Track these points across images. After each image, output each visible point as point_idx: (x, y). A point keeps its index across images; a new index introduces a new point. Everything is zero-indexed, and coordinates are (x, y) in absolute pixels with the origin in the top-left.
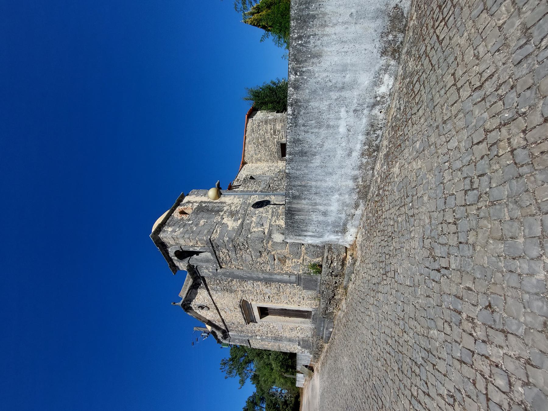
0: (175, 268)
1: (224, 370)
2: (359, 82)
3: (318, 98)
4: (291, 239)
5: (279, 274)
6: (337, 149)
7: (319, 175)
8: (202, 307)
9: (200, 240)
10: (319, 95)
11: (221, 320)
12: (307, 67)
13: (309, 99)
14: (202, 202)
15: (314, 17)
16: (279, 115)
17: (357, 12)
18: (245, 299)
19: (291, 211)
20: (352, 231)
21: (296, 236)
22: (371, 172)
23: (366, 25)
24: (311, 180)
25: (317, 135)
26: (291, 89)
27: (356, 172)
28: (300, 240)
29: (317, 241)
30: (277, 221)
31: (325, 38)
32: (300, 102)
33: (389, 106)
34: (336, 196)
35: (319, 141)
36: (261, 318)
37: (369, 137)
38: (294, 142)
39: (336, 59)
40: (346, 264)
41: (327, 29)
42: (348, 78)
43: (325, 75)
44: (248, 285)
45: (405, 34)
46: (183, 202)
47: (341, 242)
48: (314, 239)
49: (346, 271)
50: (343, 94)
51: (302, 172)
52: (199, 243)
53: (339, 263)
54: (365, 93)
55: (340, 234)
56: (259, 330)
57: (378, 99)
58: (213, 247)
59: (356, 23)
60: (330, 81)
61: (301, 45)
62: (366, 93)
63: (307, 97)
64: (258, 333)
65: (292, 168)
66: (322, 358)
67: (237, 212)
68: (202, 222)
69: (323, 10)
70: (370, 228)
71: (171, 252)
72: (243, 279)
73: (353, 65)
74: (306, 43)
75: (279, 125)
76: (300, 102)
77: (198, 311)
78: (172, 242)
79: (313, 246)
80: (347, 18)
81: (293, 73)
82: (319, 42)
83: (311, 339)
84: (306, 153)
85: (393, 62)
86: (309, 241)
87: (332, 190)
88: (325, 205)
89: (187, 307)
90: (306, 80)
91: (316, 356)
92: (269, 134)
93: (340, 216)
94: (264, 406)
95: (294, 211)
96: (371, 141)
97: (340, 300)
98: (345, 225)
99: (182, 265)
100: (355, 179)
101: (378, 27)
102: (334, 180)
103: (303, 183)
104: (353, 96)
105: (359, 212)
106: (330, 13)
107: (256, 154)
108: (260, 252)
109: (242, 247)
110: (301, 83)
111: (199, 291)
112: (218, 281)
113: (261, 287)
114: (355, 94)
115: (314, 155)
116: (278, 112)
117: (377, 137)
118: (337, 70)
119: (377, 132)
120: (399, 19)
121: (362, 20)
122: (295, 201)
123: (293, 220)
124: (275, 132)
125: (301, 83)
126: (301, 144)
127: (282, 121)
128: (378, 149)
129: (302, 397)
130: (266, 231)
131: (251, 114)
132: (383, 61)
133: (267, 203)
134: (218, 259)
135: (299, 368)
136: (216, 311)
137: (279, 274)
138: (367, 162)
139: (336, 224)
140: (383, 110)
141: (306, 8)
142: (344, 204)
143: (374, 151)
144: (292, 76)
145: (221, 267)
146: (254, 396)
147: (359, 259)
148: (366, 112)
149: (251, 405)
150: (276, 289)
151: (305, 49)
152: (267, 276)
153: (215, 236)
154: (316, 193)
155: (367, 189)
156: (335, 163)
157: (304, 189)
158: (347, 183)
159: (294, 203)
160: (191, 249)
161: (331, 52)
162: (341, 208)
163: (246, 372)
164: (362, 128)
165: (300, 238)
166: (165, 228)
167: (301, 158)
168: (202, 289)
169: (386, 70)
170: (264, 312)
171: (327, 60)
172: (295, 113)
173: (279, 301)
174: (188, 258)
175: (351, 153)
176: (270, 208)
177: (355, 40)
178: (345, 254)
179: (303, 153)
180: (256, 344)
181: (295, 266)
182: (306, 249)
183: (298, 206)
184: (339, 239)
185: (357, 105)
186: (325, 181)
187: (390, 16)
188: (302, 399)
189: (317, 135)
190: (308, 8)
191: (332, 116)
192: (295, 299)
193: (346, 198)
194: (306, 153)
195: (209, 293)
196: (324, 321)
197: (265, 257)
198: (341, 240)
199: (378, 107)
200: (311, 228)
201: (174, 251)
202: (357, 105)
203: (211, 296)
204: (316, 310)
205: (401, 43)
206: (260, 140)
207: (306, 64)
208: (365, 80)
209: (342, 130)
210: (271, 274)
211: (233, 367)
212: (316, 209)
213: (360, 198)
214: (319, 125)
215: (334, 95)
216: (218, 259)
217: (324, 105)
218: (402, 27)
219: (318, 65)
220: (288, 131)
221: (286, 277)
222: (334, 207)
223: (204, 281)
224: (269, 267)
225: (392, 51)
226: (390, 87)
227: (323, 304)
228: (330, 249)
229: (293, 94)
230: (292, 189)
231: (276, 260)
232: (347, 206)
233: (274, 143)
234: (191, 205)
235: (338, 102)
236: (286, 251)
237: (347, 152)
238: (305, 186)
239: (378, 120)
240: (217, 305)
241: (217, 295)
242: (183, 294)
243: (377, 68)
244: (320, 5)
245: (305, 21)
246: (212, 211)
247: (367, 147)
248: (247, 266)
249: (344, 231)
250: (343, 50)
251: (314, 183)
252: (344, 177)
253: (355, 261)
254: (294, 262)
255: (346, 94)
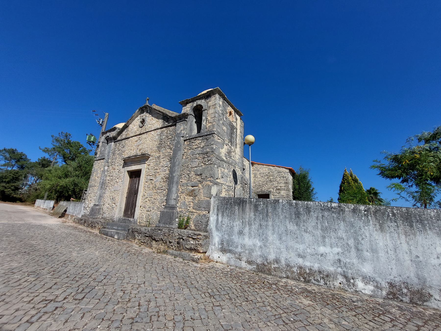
0: (186, 103)
1: (61, 135)
2: (365, 264)
3: (348, 229)
4: (214, 202)
5: (178, 190)
6: (304, 245)
7: (279, 228)
8: (143, 122)
9: (213, 126)
10: (350, 229)
11: (128, 136)
12: (372, 220)
13: (346, 221)
14: (237, 129)
15: (411, 226)
16: (291, 194)
17: (421, 262)
18: (151, 158)
19: (243, 203)
20: (224, 258)
21: (218, 206)
22: (285, 276)
23: (412, 269)
24: (274, 221)
25: (315, 227)
26: (353, 206)
27: (283, 262)
28: (214, 210)
29: (212, 224)
30: (224, 190)
31: (396, 235)
32: (343, 214)
33: (347, 291)
34: (259, 244)
35: (310, 229)
36: (128, 171)
37: (317, 273)
38: (307, 207)
39: (381, 244)
40: (191, 252)
41: (403, 237)
42: (368, 255)
43: (368, 235)
44: (165, 162)
45: (410, 303)
46: (237, 115)
47: (212, 247)
48: (215, 222)
49: (184, 253)
50: (353, 250)
51: (280, 214)
52: (210, 124)
53: (193, 246)
54: (356, 268)
55: (220, 246)
56: (114, 169)
57: (352, 281)
58: (206, 135)
59: (411, 260)
60: (362, 239)
61: (388, 215)
62: (355, 270)
63: (347, 220)
64: (111, 168)
65: (283, 205)
66: (81, 227)
67: (230, 157)
68: (225, 128)
69: (418, 234)
70: (234, 275)
71: (202, 102)
72: (172, 159)
73: (378, 258)
74: (391, 219)
75: (285, 193)
76: (343, 214)
77: (139, 118)
78: (210, 103)
79: (208, 221)
80: (415, 253)
81: (366, 209)
82: (392, 230)
83: (100, 216)
84: (298, 217)
85: (384, 293)
86: (213, 218)
87: (265, 240)
88: (250, 233)
89: (143, 110)
90: (362, 219)
91: (82, 221)
92: (277, 185)
93: (239, 246)
94: (15, 168)
95: (243, 205)
96: (313, 275)
97: (151, 247)
98: (230, 251)
99: (187, 109)
100: (277, 261)
101: (411, 279)
102: (274, 241)
103: (270, 214)
104: (352, 258)
105: (243, 264)
106: (416, 240)
107: (260, 174)
108: (201, 174)
109: (206, 159)
110: (359, 215)
111: (161, 121)
112: (170, 137)
113: (164, 173)
114: (354, 260)
115: (297, 225)
116: (293, 192)
117: (318, 281)
118: (372, 245)
119: (322, 281)
120: (421, 298)
121: (415, 266)
122: (252, 207)
123: (231, 205)
124: (278, 189)
125: (359, 215)
126: (306, 213)
127: (288, 196)
128: (307, 281)
129: (22, 205)
130: (218, 181)
131: (292, 173)
132: (384, 284)
133: (236, 183)
134: (193, 138)
135: (63, 203)
136: (138, 133)
137: (178, 190)
138: (293, 272)
139: (231, 243)
140: (342, 285)
141: (417, 220)
142: (251, 251)
143: (305, 278)
144: (363, 207)
145: (185, 141)
146: (26, 159)
147: (199, 265)
148: (339, 270)
149: (18, 157)
150: (161, 186)
151: (386, 218)
152: (175, 179)
153: (216, 137)
154: (261, 225)
155: (268, 272)
156: (291, 243)
157: (265, 214)
158: (272, 253)
159: (250, 206)
160: (204, 118)
161: (386, 240)
162: (247, 247)
163: (55, 154)
164: (325, 267)
165: (216, 210)
166: (221, 100)
167: (293, 213)
168: (162, 124)
169: (377, 287)
170: (135, 175)
171: (379, 236)
172: (333, 209)
173: (146, 188)
174: (194, 115)
175: (301, 257)
176: (233, 184)
177: (398, 260)
178: (201, 251)
179: (298, 215)
180: (98, 168)
181: (184, 204)
182: (204, 215)
183: (247, 209)
184: (215, 245)
185: (345, 262)
186: (273, 234)
187: (422, 290)
188: (19, 205)
189: (315, 227)
190: (417, 222)
191: (333, 240)
192: (148, 203)
193: (257, 253)
194: (298, 217)
195: (158, 129)
196: (125, 230)
197: (196, 179)
198: (213, 247)
199: (344, 281)
200: (226, 220)
201: (202, 104)
202: (345, 262)
203: (155, 130)
204: (135, 223)
205: (402, 301)
206: (271, 177)
207: (374, 219)
208: (367, 269)
209: (322, 249)
210: (177, 183)
211: (62, 143)
212: (246, 225)
213: (258, 265)
214: (324, 229)
215: (351, 242)
216: (193, 138)
217: (341, 233)
218: (415, 301)
219: (375, 229)
220: (317, 203)
221: (174, 196)
222: (248, 241)
223: (171, 126)
224: (184, 181)
225: (394, 292)
226: (363, 291)
227: (145, 229)
228: (206, 237)
229: (348, 208)
230: (264, 204)
231: (192, 188)
232: (249, 253)
233: (269, 188)
234: (235, 121)
235: (345, 245)
236: (202, 197)
237: (302, 254)
238: (267, 215)
239: (333, 281)
240: (145, 134)
241: (155, 135)
242: (155, 107)
243: (378, 279)
244: (421, 231)
245: (407, 219)
246: (232, 137)
247: (308, 271)
248: (186, 162)
249: (223, 250)
250: (389, 250)
251: (270, 223)
252: (278, 251)
253: (196, 261)
254: (190, 204)
255: (353, 251)
